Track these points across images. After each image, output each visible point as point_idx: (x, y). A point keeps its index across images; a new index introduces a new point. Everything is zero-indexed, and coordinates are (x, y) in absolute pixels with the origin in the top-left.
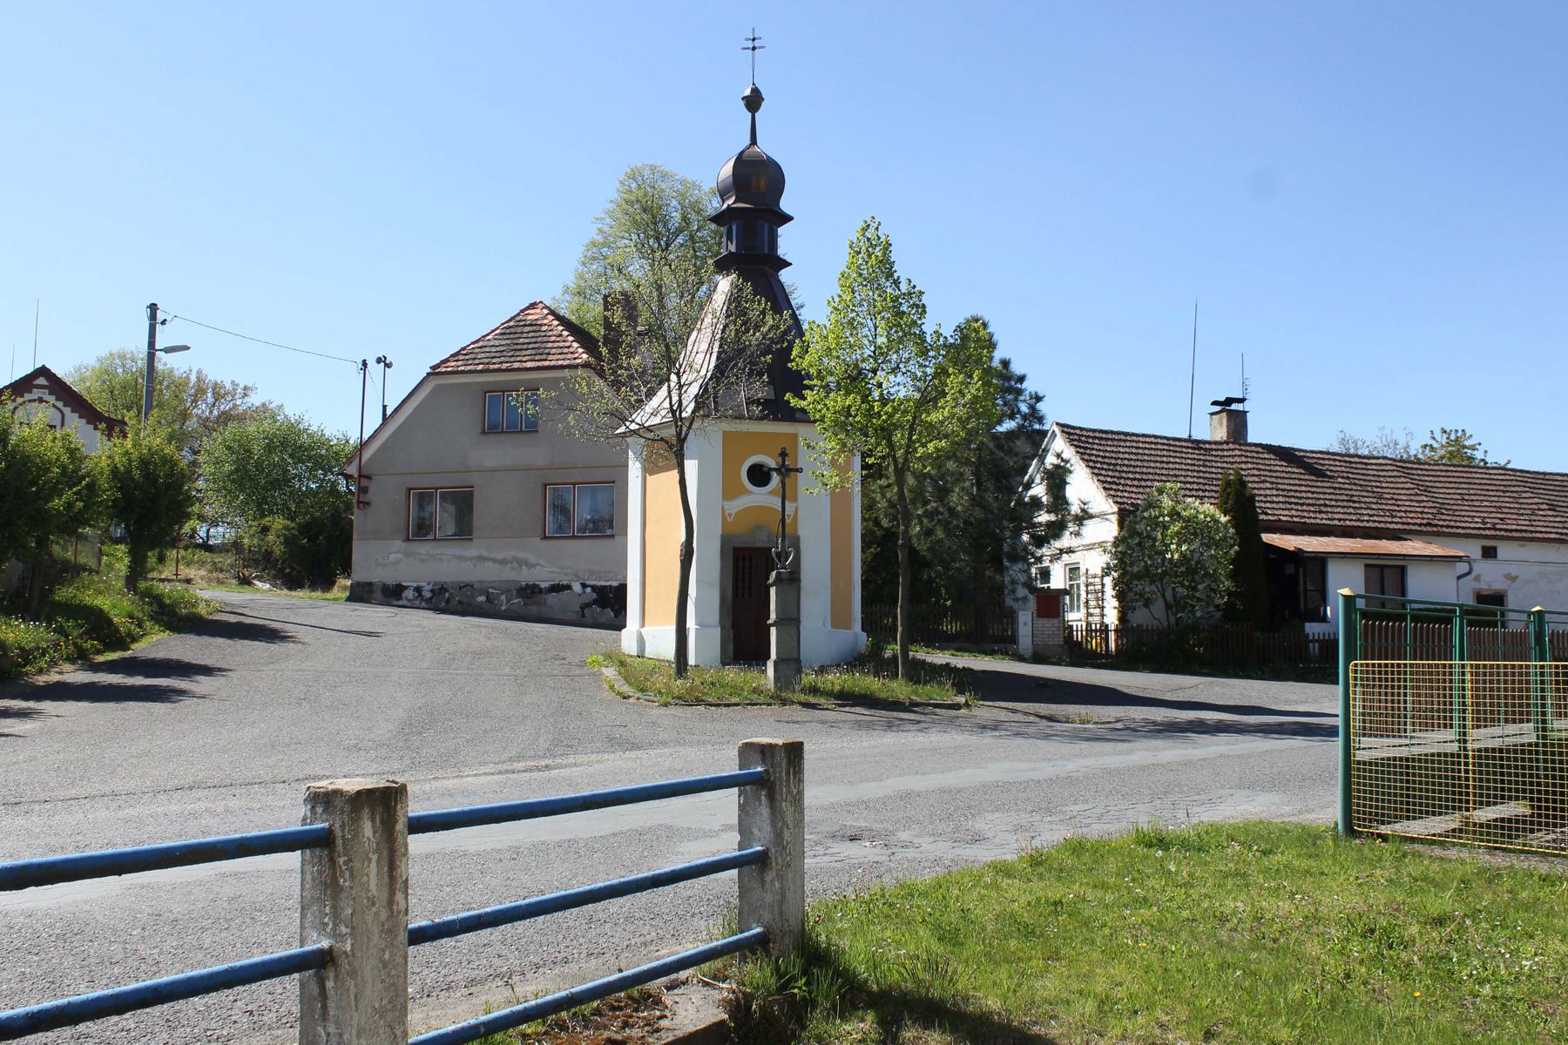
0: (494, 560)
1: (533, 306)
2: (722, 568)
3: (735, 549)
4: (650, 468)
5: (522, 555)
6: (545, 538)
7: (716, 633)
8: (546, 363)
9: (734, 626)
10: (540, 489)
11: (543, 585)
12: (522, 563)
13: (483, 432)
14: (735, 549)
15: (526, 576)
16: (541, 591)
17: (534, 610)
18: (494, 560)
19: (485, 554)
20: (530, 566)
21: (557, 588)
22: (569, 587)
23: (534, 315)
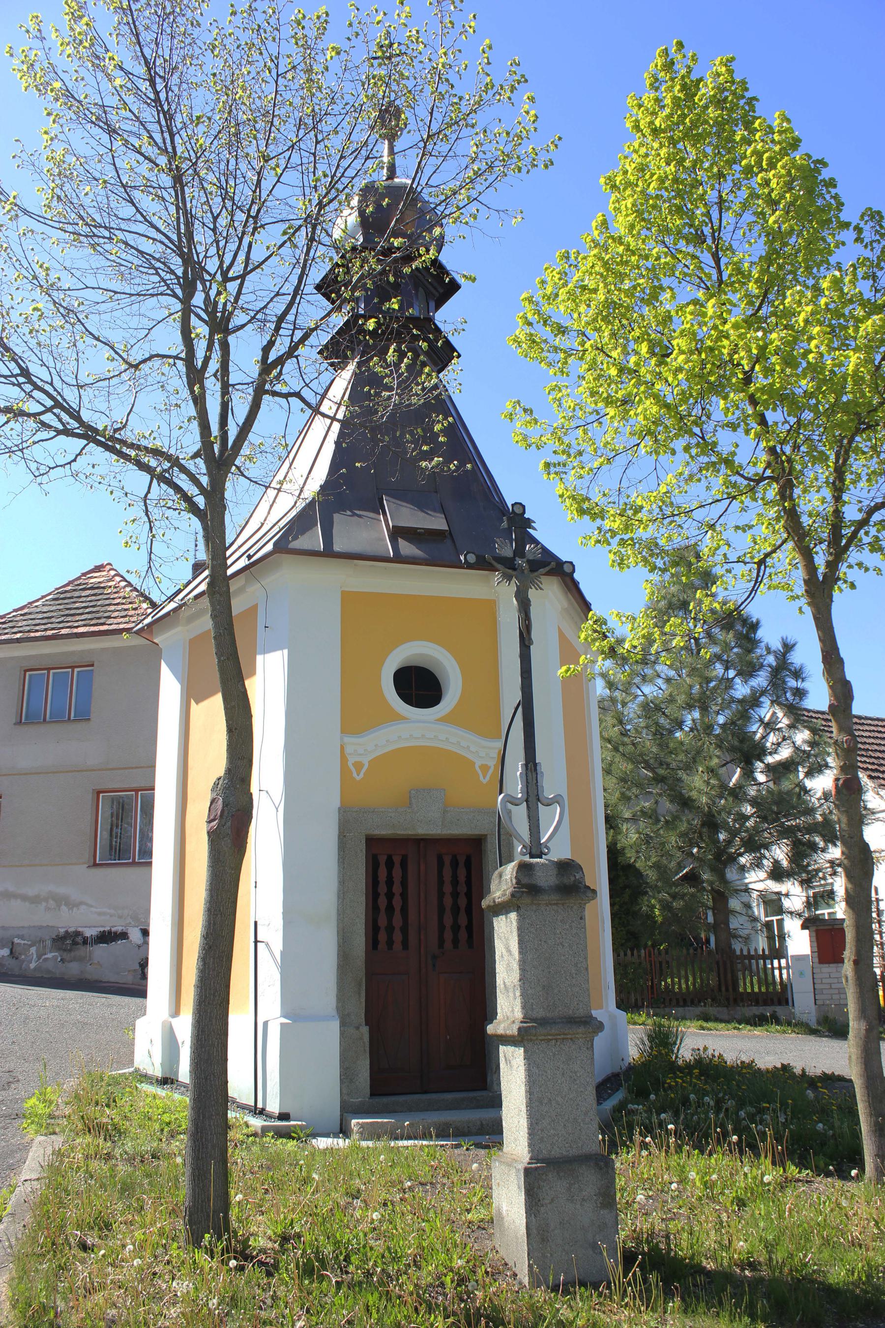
0: (24, 898)
1: (98, 568)
2: (342, 882)
3: (371, 841)
4: (193, 693)
5: (62, 890)
6: (95, 865)
7: (330, 1033)
8: (105, 628)
9: (375, 1016)
10: (89, 797)
11: (89, 933)
12: (61, 901)
13: (20, 723)
14: (371, 841)
15: (67, 920)
16: (85, 941)
17: (74, 969)
18: (24, 898)
19: (11, 888)
20: (72, 905)
21: (107, 937)
22: (124, 935)
23: (97, 579)
